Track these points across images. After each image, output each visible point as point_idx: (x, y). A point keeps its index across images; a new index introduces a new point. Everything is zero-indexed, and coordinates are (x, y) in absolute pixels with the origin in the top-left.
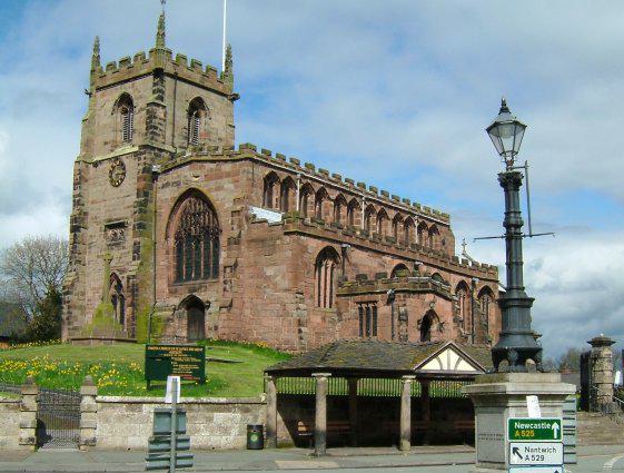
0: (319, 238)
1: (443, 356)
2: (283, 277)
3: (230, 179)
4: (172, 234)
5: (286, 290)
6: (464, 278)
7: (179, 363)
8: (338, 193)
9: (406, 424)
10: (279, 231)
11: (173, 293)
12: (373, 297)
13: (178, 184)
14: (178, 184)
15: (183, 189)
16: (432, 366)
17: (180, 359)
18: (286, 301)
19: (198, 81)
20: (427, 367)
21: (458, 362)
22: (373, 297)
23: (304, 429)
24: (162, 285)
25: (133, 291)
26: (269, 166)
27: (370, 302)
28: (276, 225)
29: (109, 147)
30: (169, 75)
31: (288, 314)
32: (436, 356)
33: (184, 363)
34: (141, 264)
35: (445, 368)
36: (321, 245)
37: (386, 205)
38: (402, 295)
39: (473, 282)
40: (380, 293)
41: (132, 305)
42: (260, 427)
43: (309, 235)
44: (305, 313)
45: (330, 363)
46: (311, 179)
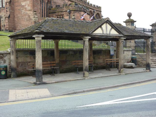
1: (104, 26)
2: (28, 5)
5: (30, 10)
6: (91, 10)
9: (86, 63)
16: (99, 32)
18: (30, 14)
20: (95, 32)
21: (111, 29)
22: (62, 13)
27: (61, 15)
31: (31, 19)
35: (105, 33)
38: (73, 12)
39: (94, 12)
42: (6, 67)
44: (37, 19)
45: (44, 30)
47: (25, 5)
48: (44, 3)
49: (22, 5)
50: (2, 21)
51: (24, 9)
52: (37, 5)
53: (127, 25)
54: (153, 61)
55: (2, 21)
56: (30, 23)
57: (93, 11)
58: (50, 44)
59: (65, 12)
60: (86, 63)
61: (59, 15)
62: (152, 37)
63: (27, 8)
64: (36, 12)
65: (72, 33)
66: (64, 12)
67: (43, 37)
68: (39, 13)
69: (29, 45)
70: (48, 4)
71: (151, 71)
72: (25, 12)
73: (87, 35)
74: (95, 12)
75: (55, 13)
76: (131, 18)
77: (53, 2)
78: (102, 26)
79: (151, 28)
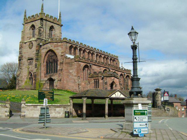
0: (84, 62)
1: (116, 93)
2: (74, 73)
3: (60, 47)
4: (45, 61)
5: (75, 76)
6: (122, 73)
7: (47, 95)
8: (89, 50)
9: (107, 111)
10: (73, 61)
12: (98, 78)
13: (47, 48)
14: (47, 48)
15: (48, 49)
16: (114, 96)
17: (47, 94)
18: (75, 79)
19: (52, 21)
21: (120, 95)
22: (98, 78)
23: (80, 112)
24: (43, 75)
25: (35, 76)
26: (71, 43)
27: (97, 79)
30: (44, 20)
31: (76, 82)
33: (48, 95)
34: (37, 69)
35: (117, 96)
37: (101, 54)
38: (106, 77)
40: (100, 77)
42: (68, 112)
43: (81, 62)
44: (80, 82)
45: (87, 95)
46: (82, 47)
56: (75, 85)
58: (89, 101)
60: (107, 111)
74: (125, 74)
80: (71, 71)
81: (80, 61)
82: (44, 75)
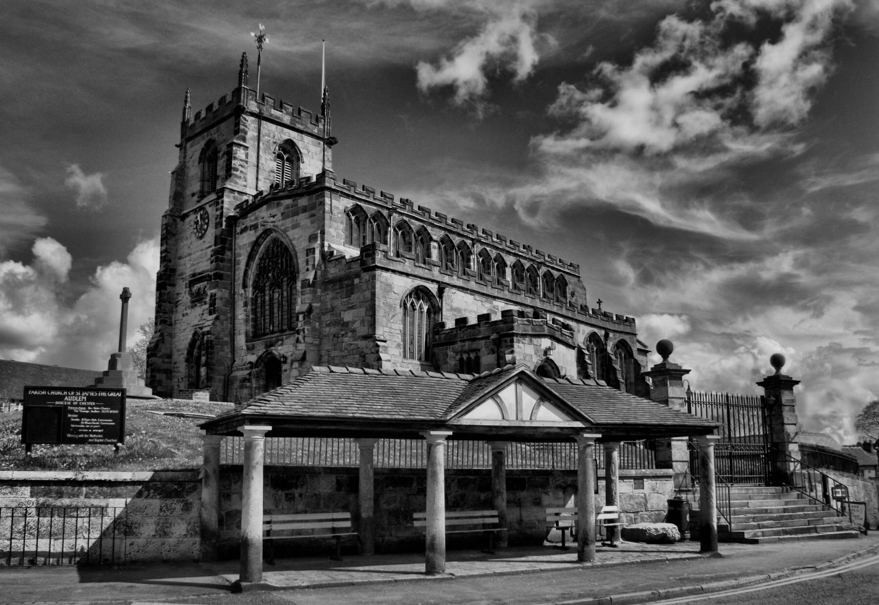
0: (408, 275)
1: (508, 394)
2: (363, 322)
3: (307, 214)
4: (250, 283)
6: (596, 330)
7: (81, 415)
8: (443, 233)
10: (356, 267)
11: (250, 349)
12: (475, 345)
13: (255, 227)
14: (255, 227)
15: (260, 230)
17: (82, 410)
18: (366, 351)
19: (288, 123)
22: (475, 345)
23: (51, 562)
24: (241, 340)
25: (207, 349)
26: (353, 197)
27: (472, 351)
28: (354, 260)
29: (196, 198)
30: (252, 114)
32: (494, 395)
33: (90, 416)
34: (217, 318)
36: (409, 284)
37: (503, 250)
40: (482, 339)
41: (207, 364)
43: (394, 271)
46: (407, 216)
47: (354, 322)
48: (417, 313)
49: (345, 320)
50: (286, 371)
51: (350, 334)
52: (392, 321)
53: (658, 383)
54: (771, 513)
55: (286, 371)
57: (603, 332)
59: (483, 341)
61: (465, 352)
62: (717, 427)
63: (357, 330)
64: (385, 341)
65: (396, 420)
66: (481, 342)
67: (269, 431)
68: (399, 345)
69: (742, 426)
70: (432, 315)
71: (720, 556)
72: (351, 344)
73: (440, 425)
75: (454, 343)
76: (673, 359)
77: (449, 308)
78: (499, 394)
79: (760, 391)
80: (347, 316)
81: (387, 270)
82: (247, 341)
